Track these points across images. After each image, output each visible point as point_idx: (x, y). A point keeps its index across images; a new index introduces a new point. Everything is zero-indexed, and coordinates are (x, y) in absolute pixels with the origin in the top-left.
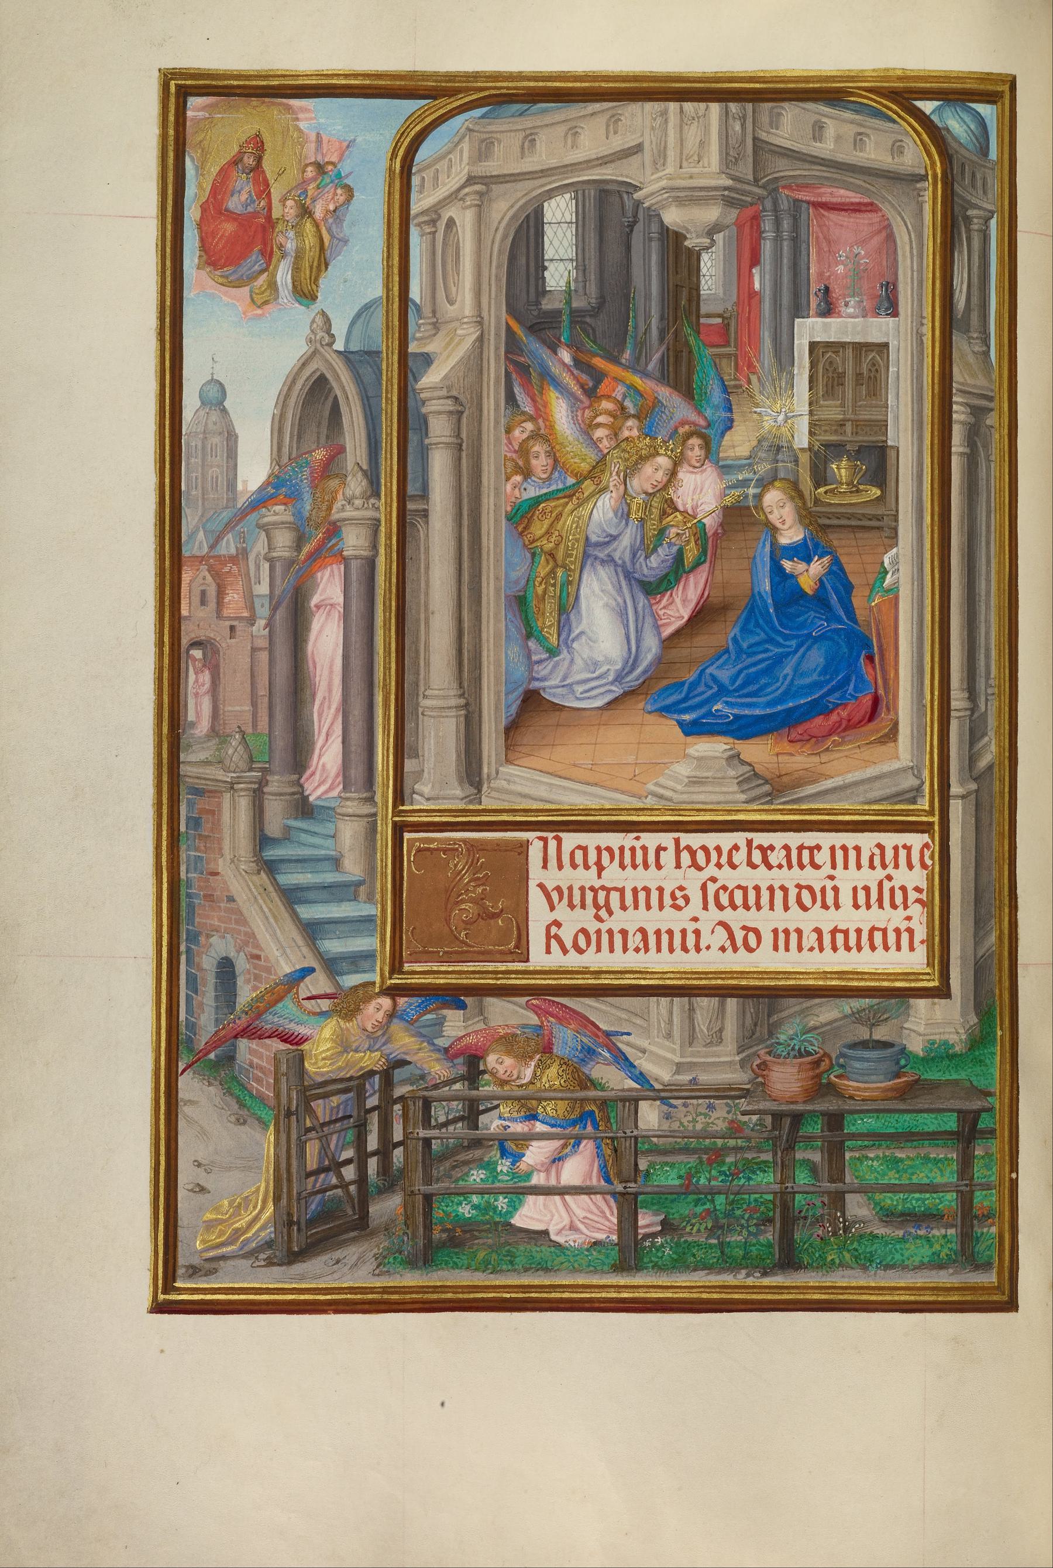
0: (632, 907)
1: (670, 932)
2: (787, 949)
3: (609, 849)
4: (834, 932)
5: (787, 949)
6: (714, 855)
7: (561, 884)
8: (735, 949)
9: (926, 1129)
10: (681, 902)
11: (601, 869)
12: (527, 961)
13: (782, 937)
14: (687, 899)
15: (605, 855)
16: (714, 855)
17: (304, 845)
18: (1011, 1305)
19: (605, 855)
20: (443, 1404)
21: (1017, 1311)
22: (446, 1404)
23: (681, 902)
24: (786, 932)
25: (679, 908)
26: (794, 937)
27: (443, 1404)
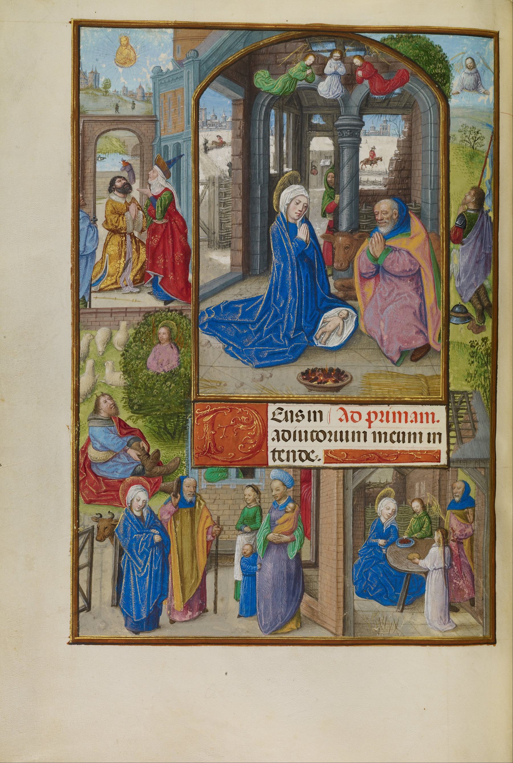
1: (306, 432)
3: (375, 413)
11: (369, 421)
12: (440, 462)
13: (356, 435)
15: (373, 416)
16: (328, 435)
18: (492, 641)
19: (373, 416)
20: (226, 674)
22: (228, 674)
23: (300, 418)
24: (380, 433)
26: (418, 436)
27: (226, 674)
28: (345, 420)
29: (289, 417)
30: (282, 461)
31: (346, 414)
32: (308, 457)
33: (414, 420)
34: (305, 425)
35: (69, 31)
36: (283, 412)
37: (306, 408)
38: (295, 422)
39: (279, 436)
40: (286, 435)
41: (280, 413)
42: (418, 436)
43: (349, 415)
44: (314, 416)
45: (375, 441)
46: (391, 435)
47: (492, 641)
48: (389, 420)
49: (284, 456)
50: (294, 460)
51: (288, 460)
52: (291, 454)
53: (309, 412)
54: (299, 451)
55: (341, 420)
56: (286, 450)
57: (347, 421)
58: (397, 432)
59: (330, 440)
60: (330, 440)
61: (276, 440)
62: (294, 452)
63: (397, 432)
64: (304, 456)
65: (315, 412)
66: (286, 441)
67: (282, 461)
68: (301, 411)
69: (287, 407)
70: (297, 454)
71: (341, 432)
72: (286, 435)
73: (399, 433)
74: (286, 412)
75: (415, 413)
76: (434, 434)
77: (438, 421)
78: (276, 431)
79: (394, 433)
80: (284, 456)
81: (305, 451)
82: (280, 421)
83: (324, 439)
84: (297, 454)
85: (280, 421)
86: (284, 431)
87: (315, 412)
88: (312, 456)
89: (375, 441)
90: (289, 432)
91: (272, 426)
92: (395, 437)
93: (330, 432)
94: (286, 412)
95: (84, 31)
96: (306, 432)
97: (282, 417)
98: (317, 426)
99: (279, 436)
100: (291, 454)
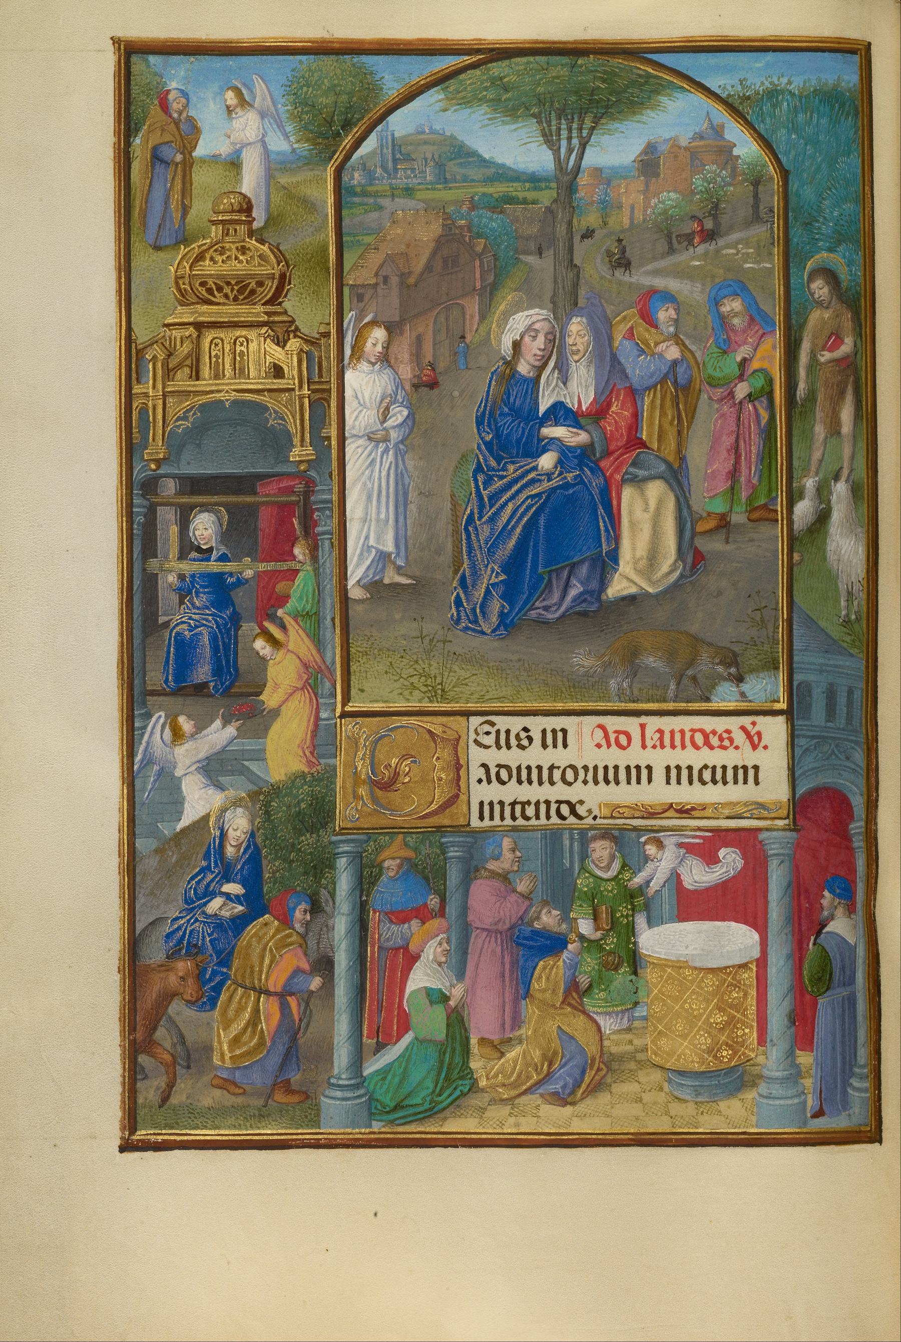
0: (551, 746)
1: (539, 768)
2: (679, 783)
4: (552, 768)
5: (679, 783)
6: (582, 773)
7: (663, 728)
8: (489, 782)
9: (138, 993)
10: (525, 742)
13: (634, 772)
14: (530, 739)
16: (582, 773)
17: (291, 695)
18: (875, 1136)
20: (376, 1214)
21: (880, 1141)
22: (378, 1214)
23: (525, 742)
24: (638, 768)
25: (523, 748)
26: (751, 773)
27: (376, 1214)
28: (605, 746)
29: (504, 741)
30: (528, 819)
31: (607, 736)
32: (573, 812)
33: (658, 744)
34: (535, 756)
35: (108, 61)
36: (493, 730)
37: (536, 724)
38: (514, 748)
39: (489, 775)
40: (504, 774)
41: (488, 733)
42: (751, 773)
43: (612, 737)
44: (561, 738)
45: (668, 783)
46: (700, 772)
47: (875, 1136)
48: (676, 744)
49: (530, 811)
50: (548, 817)
51: (538, 817)
52: (543, 808)
53: (544, 732)
54: (557, 802)
55: (599, 746)
56: (533, 801)
57: (609, 746)
58: (711, 765)
59: (585, 782)
60: (585, 782)
61: (485, 782)
62: (548, 803)
63: (711, 765)
64: (565, 810)
65: (554, 731)
66: (503, 783)
67: (528, 819)
68: (526, 730)
69: (502, 722)
70: (554, 807)
71: (606, 768)
72: (504, 774)
73: (714, 768)
74: (498, 732)
75: (661, 732)
76: (735, 768)
77: (765, 747)
78: (484, 766)
79: (706, 767)
80: (530, 811)
81: (568, 803)
82: (487, 747)
83: (575, 781)
84: (554, 807)
85: (487, 747)
86: (499, 766)
87: (554, 731)
88: (581, 810)
89: (668, 783)
90: (508, 768)
91: (477, 756)
92: (707, 775)
93: (586, 768)
94: (498, 732)
95: (134, 59)
96: (539, 768)
97: (490, 740)
98: (559, 757)
99: (489, 775)
100: (543, 808)
